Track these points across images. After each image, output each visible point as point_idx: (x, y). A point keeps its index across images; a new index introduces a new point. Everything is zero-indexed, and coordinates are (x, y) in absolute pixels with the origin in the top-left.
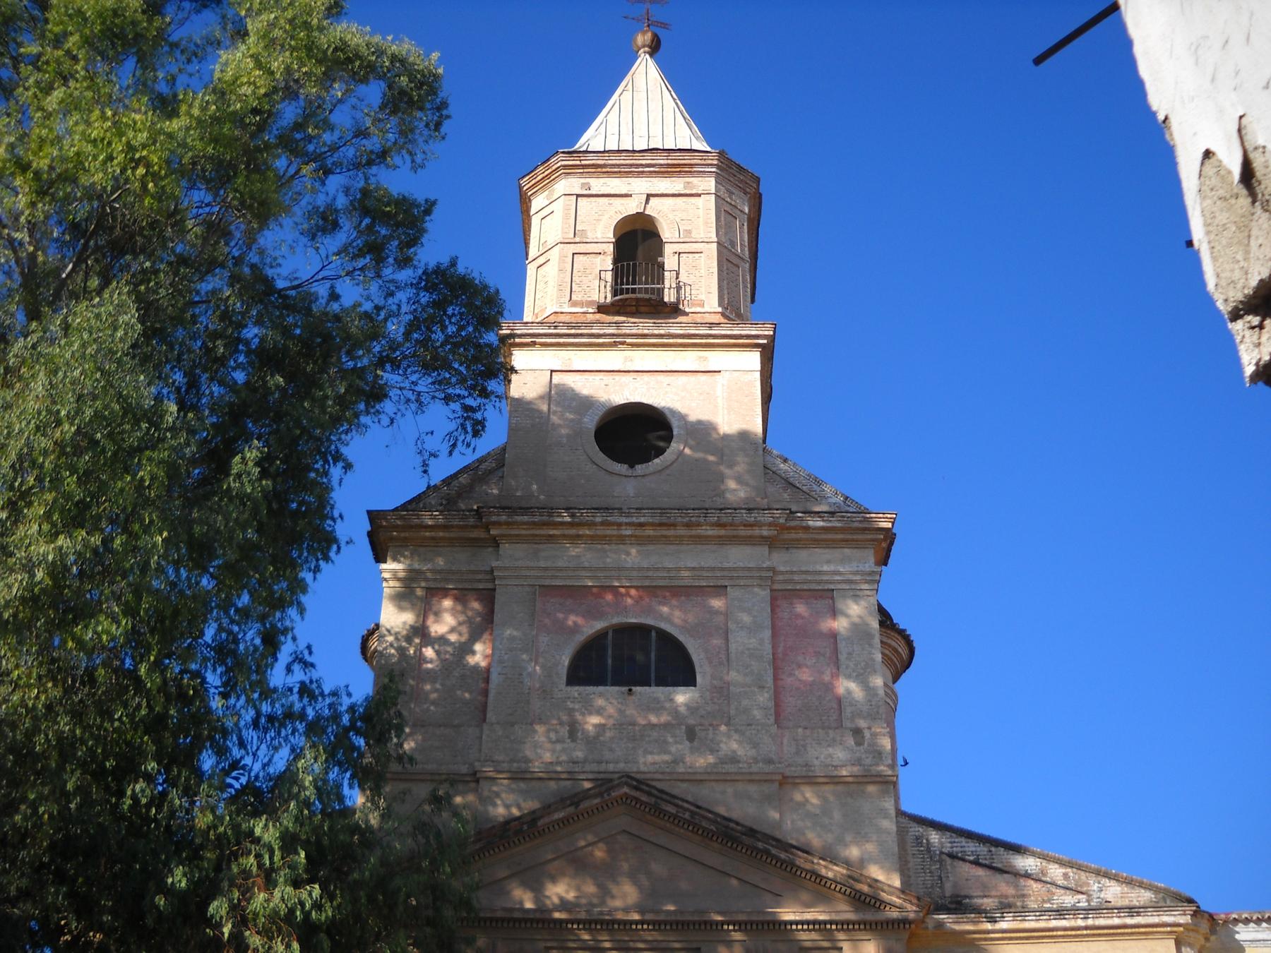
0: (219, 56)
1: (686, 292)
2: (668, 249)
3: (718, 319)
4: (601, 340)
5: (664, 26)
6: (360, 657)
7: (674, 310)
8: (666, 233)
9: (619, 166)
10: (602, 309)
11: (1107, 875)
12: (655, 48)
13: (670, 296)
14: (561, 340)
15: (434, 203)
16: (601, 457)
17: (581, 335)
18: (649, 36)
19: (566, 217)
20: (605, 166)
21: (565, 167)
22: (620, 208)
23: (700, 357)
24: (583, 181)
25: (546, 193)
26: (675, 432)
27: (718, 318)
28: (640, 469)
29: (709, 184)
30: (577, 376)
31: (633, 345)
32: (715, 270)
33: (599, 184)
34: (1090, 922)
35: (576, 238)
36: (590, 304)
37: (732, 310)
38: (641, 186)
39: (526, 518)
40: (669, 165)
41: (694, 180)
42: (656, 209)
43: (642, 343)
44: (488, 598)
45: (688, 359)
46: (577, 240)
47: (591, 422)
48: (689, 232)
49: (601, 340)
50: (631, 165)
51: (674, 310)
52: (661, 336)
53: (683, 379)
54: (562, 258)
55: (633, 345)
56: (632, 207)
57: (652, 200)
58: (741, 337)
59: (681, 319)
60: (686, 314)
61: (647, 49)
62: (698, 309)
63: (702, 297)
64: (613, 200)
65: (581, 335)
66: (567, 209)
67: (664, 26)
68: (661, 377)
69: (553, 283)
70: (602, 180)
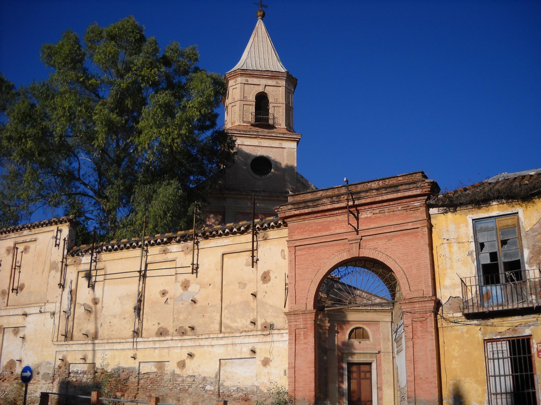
0: (173, 374)
1: (276, 120)
2: (271, 106)
3: (287, 132)
4: (253, 136)
5: (266, 7)
6: (200, 266)
7: (272, 127)
8: (271, 100)
9: (257, 75)
10: (252, 125)
11: (377, 296)
12: (263, 16)
13: (271, 122)
14: (241, 135)
15: (251, 294)
16: (252, 173)
17: (247, 134)
18: (262, 13)
19: (241, 92)
20: (253, 74)
21: (241, 74)
22: (257, 89)
23: (280, 143)
24: (246, 78)
25: (234, 80)
26: (273, 167)
27: (285, 131)
28: (263, 177)
29: (283, 83)
30: (246, 147)
31: (261, 138)
32: (285, 113)
33: (252, 80)
34: (372, 308)
35: (244, 99)
36: (249, 122)
37: (290, 127)
38: (263, 82)
39: (233, 193)
40: (272, 76)
41: (279, 81)
42: (268, 90)
43: (264, 137)
44: (223, 214)
45: (276, 144)
46: (245, 100)
47: (249, 162)
48: (277, 99)
49: (253, 136)
50: (261, 75)
51: (272, 127)
52: (269, 136)
53: (275, 149)
54: (240, 106)
55: (261, 138)
56: (260, 89)
57: (267, 87)
58: (292, 138)
59: (275, 130)
60: (276, 128)
61: (261, 17)
62: (280, 127)
63: (281, 122)
64: (255, 86)
65: (247, 134)
66: (241, 88)
67: (266, 7)
68: (269, 149)
69: (237, 114)
70: (252, 79)
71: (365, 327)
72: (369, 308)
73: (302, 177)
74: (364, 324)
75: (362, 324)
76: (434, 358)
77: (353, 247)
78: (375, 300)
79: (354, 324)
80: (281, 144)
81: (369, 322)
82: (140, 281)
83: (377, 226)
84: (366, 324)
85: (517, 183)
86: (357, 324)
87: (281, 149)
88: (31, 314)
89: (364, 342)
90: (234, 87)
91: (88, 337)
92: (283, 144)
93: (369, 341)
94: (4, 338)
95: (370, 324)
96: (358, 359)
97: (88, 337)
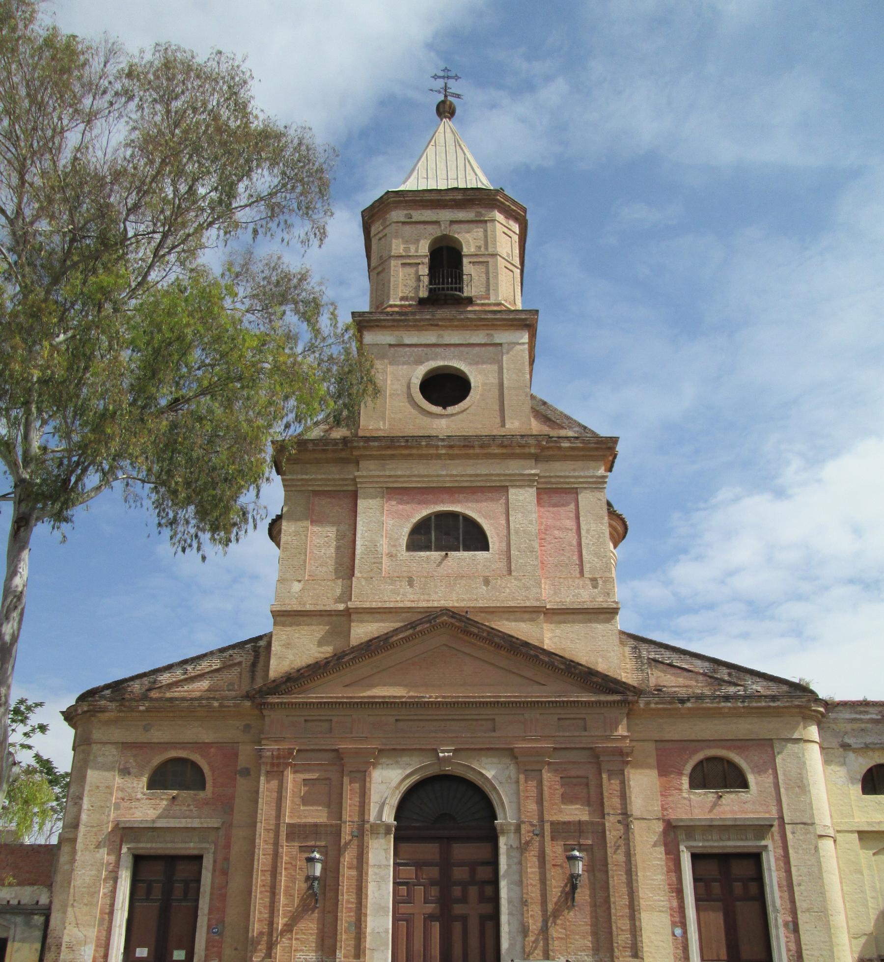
23: (488, 334)
28: (450, 410)
38: (445, 215)
53: (477, 349)
62: (486, 301)
73: (545, 403)
74: (729, 748)
75: (723, 748)
76: (384, 909)
79: (702, 749)
80: (492, 335)
81: (742, 744)
82: (273, 705)
85: (851, 923)
86: (710, 747)
87: (491, 348)
88: (852, 832)
90: (380, 235)
92: (495, 335)
94: (846, 834)
96: (721, 844)
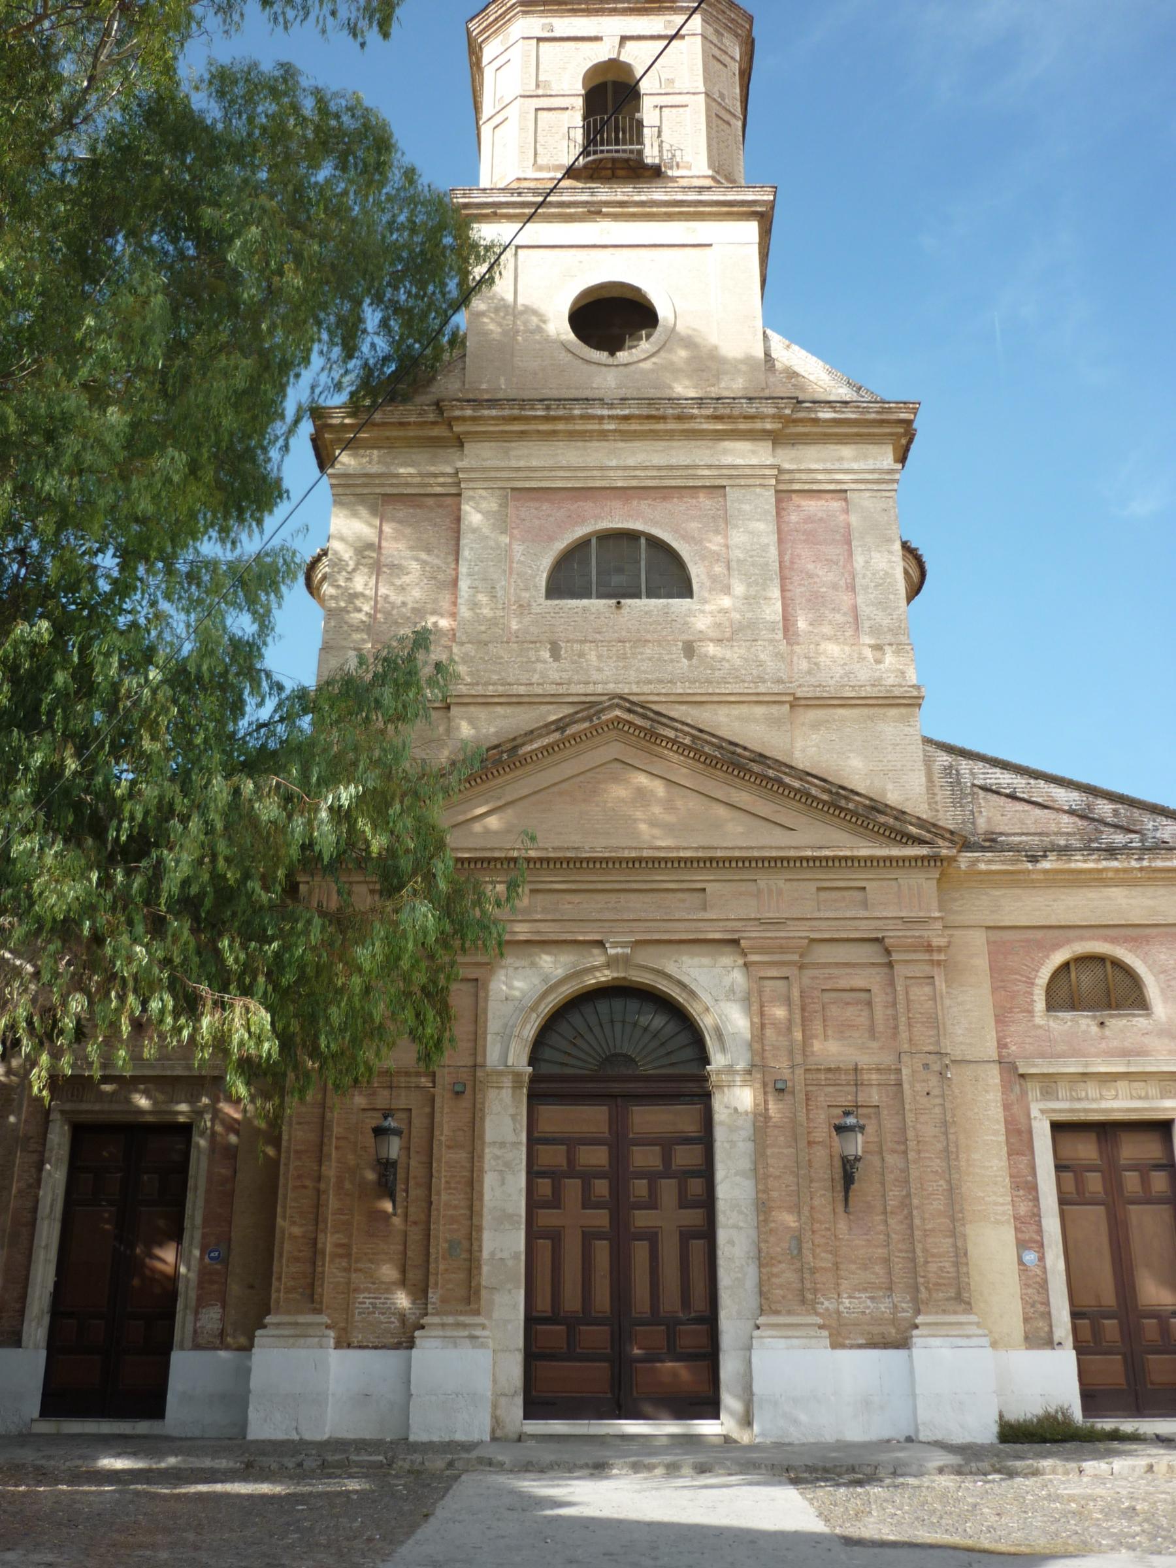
7: (656, 173)
28: (622, 356)
34: (1145, 863)
39: (494, 412)
42: (636, 56)
46: (540, 92)
48: (671, 81)
52: (642, 204)
56: (602, 53)
71: (1122, 953)
72: (1134, 864)
74: (1113, 940)
75: (1106, 939)
77: (497, 1158)
78: (1156, 829)
79: (1068, 941)
83: (1030, 932)
84: (1126, 940)
86: (1082, 939)
89: (1123, 1022)
91: (915, 588)
93: (1149, 1016)
95: (1147, 940)
97: (915, 588)
